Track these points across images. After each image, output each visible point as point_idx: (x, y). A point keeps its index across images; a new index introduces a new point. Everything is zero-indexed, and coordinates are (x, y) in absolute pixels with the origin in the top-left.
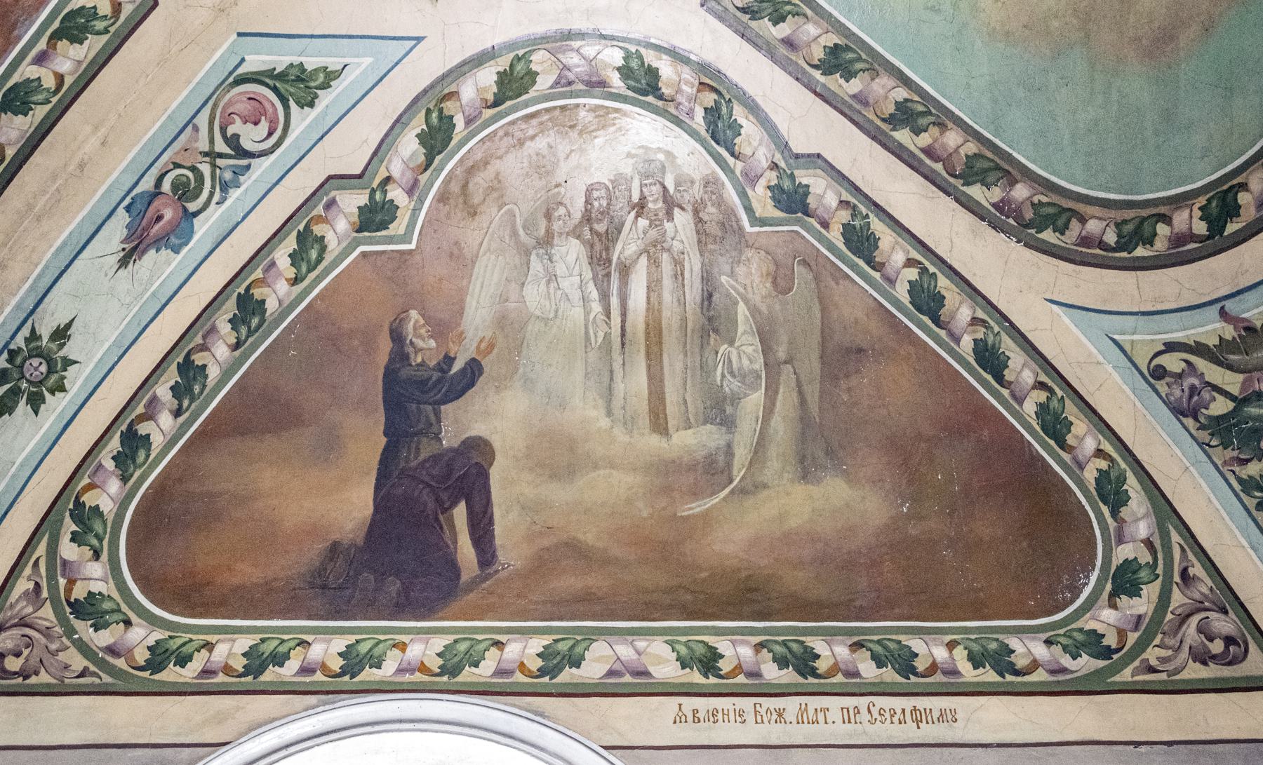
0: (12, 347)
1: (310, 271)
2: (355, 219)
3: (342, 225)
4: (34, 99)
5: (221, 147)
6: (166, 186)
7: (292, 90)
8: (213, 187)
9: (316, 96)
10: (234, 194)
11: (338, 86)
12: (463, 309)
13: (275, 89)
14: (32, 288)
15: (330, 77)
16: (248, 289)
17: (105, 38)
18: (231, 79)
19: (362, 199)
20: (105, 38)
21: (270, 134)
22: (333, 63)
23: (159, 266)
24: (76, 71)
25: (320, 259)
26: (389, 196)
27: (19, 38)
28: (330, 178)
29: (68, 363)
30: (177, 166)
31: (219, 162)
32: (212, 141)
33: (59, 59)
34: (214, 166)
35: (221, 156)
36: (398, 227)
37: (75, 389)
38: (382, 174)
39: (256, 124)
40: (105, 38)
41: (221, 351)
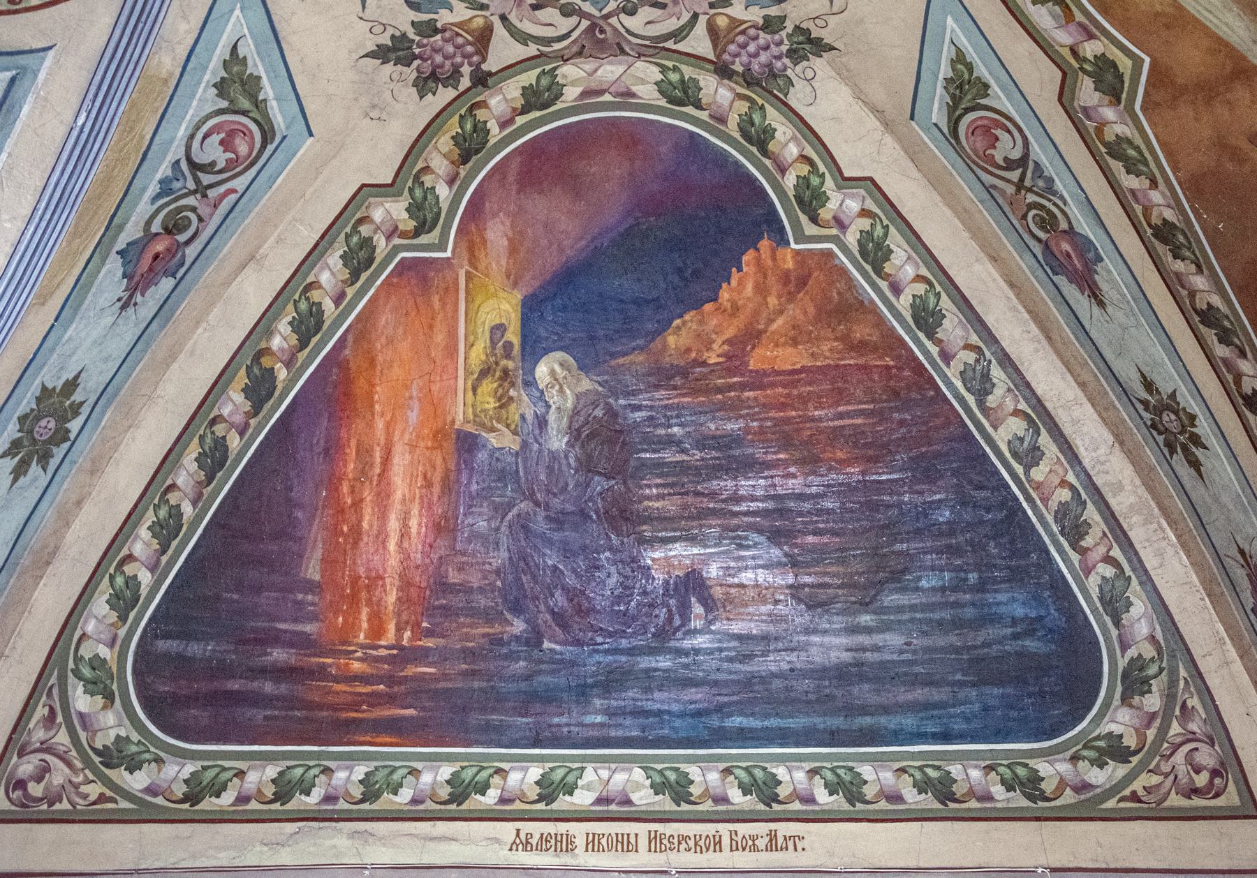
0: (1149, 423)
1: (1147, 165)
2: (1107, 99)
3: (1109, 113)
4: (931, 306)
5: (1015, 175)
6: (1042, 235)
7: (969, 97)
8: (1050, 200)
9: (978, 78)
10: (1058, 185)
11: (971, 54)
12: (1227, 45)
13: (967, 110)
14: (1106, 379)
15: (960, 58)
16: (1150, 226)
17: (892, 230)
18: (953, 141)
19: (1087, 84)
20: (892, 229)
21: (1009, 132)
22: (947, 53)
23: (1109, 275)
24: (917, 263)
25: (1137, 149)
26: (1090, 57)
27: (872, 302)
28: (1060, 100)
29: (1173, 395)
30: (1025, 217)
31: (1028, 183)
32: (1008, 181)
33: (901, 275)
34: (1029, 190)
35: (1022, 179)
36: (1125, 64)
37: (1196, 409)
38: (1066, 53)
39: (997, 139)
40: (892, 230)
41: (1200, 282)
